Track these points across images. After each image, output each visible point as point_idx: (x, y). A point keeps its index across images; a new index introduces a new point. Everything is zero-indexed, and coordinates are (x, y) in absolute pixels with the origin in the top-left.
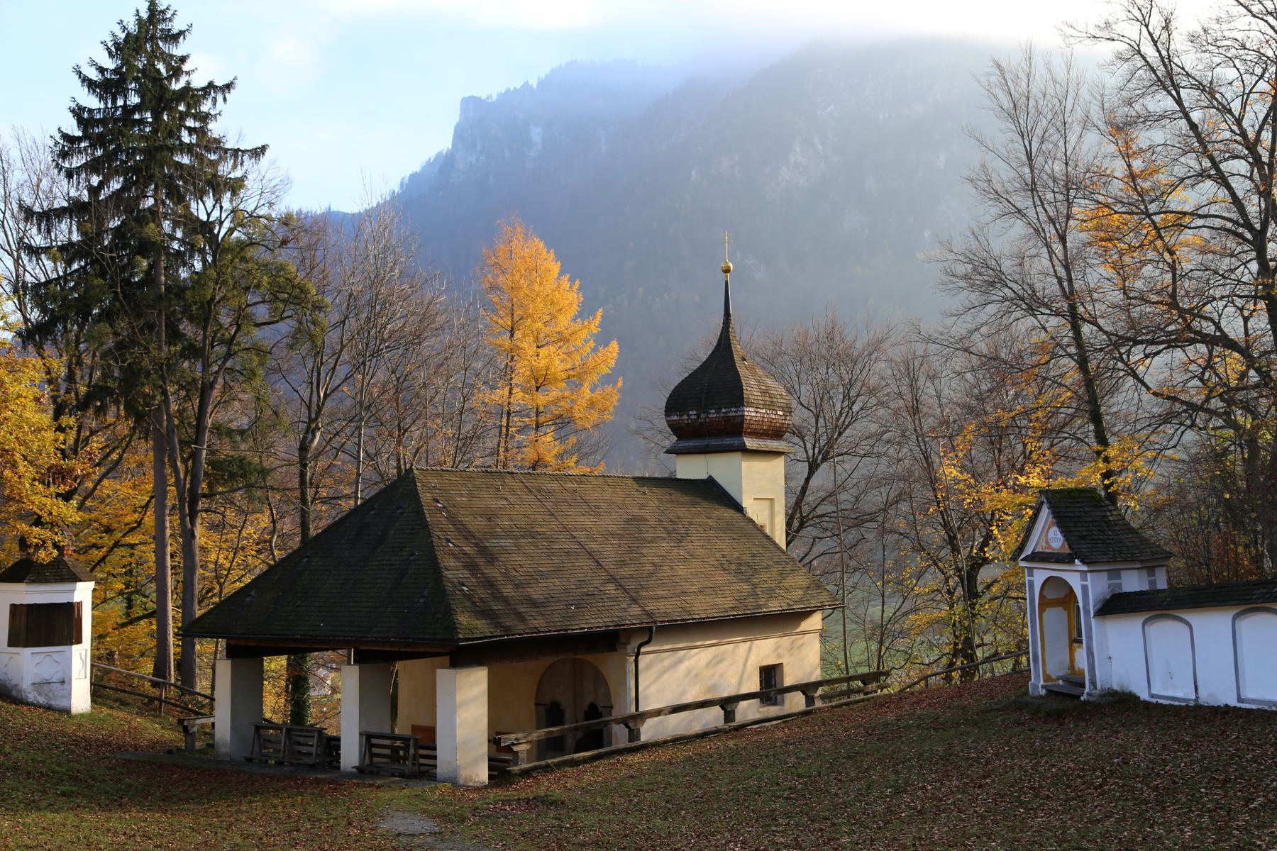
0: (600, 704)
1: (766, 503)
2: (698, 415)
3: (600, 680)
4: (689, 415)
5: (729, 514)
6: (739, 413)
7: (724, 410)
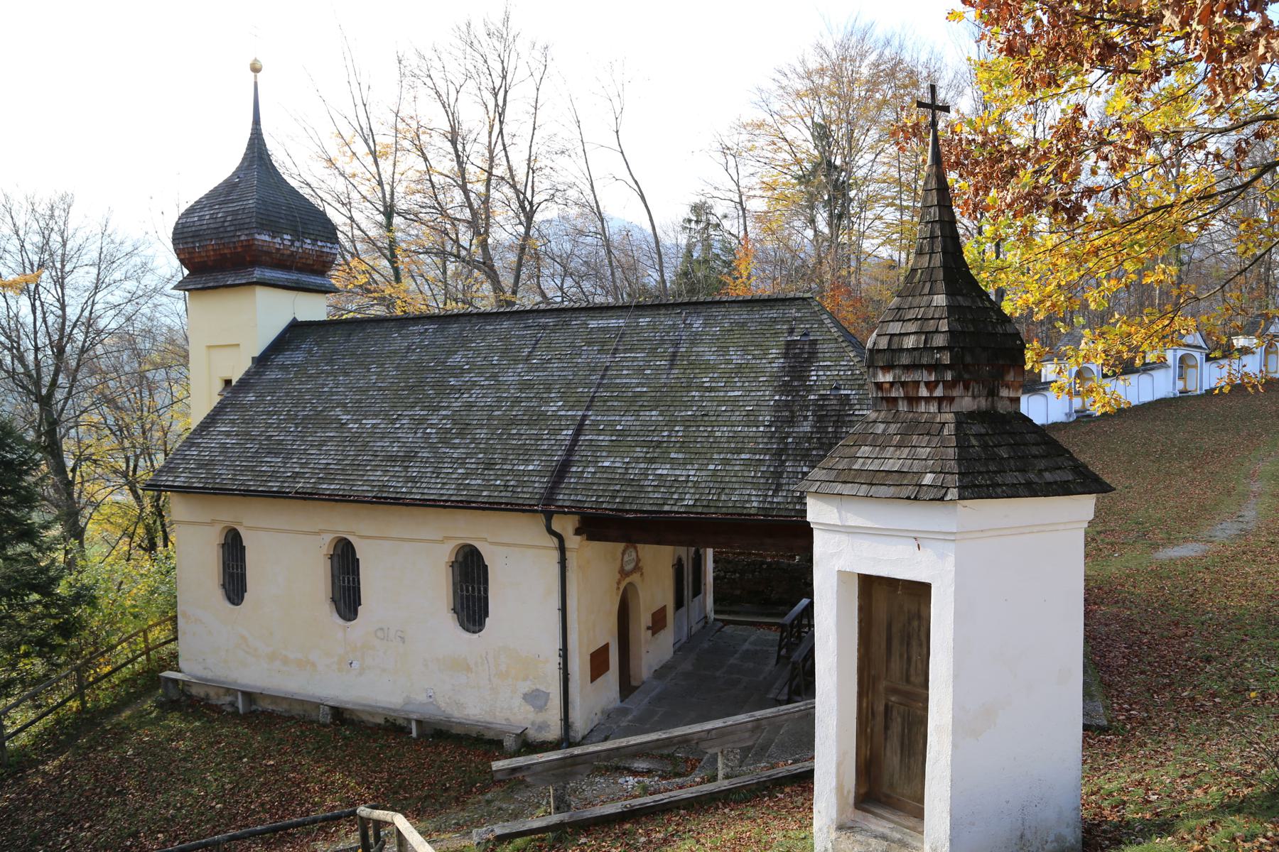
2: (292, 242)
4: (283, 239)
7: (319, 243)
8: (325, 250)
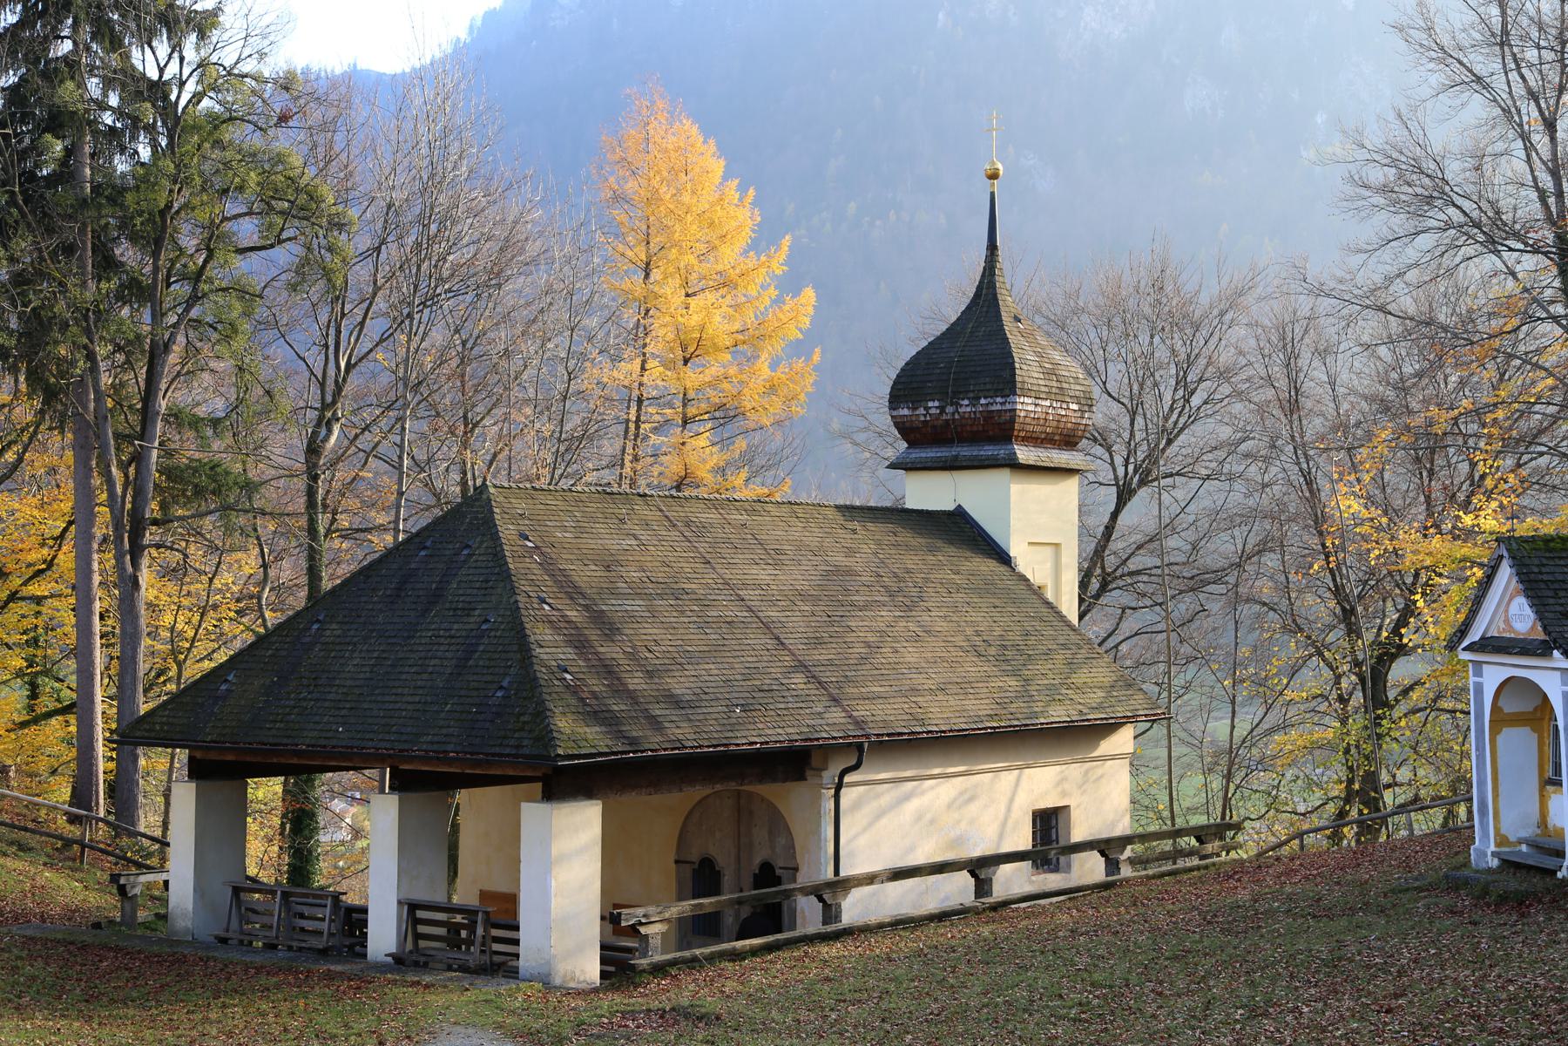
0: (779, 863)
1: (1049, 551)
2: (942, 409)
3: (778, 824)
4: (927, 409)
5: (988, 566)
6: (1008, 407)
7: (983, 401)
8: (994, 408)
